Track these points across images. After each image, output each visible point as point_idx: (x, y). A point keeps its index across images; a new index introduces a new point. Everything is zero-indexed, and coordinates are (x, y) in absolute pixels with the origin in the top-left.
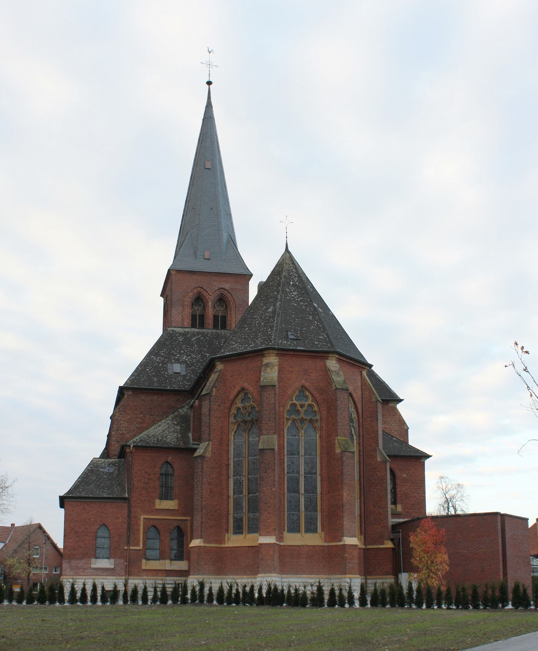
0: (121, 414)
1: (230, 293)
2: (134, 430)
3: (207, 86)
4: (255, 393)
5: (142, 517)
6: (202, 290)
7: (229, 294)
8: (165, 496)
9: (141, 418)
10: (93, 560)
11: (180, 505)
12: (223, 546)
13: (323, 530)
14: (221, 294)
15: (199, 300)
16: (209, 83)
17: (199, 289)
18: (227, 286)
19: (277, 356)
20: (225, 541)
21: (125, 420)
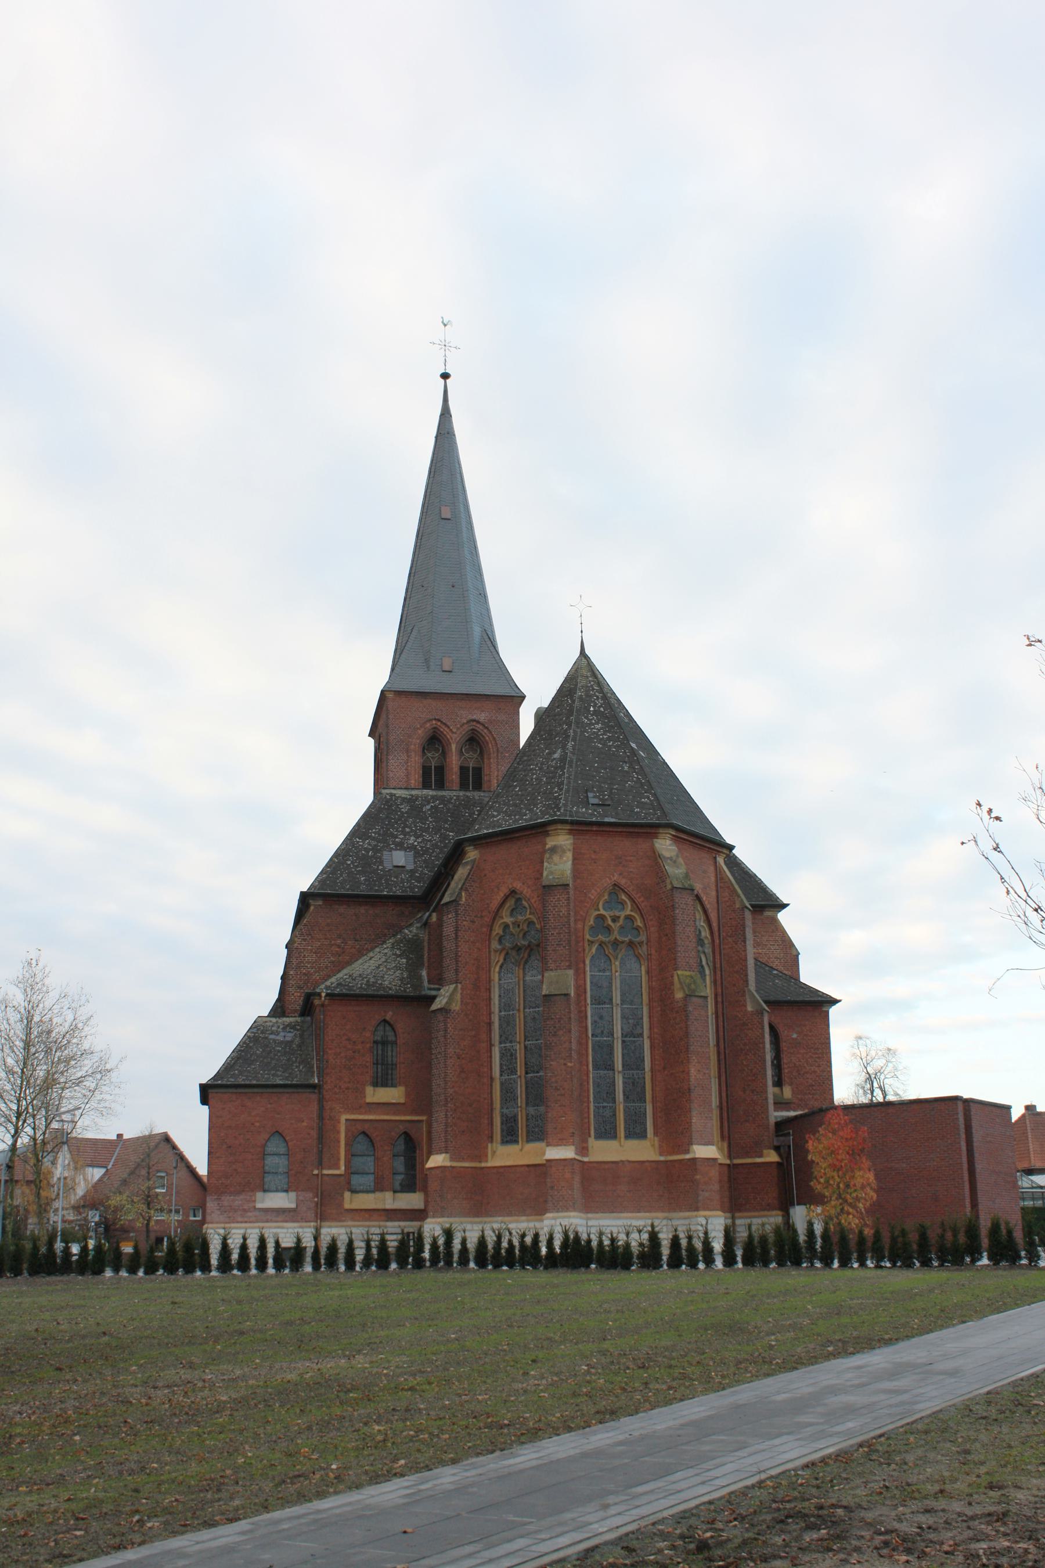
0: (305, 940)
1: (487, 728)
2: (326, 967)
3: (442, 381)
4: (533, 898)
5: (343, 1118)
6: (439, 723)
7: (485, 731)
8: (383, 1081)
9: (339, 946)
10: (259, 1195)
11: (408, 1095)
12: (483, 1165)
13: (656, 1134)
14: (473, 729)
15: (435, 741)
16: (445, 376)
17: (434, 722)
18: (482, 717)
19: (569, 834)
20: (487, 1156)
21: (311, 950)
